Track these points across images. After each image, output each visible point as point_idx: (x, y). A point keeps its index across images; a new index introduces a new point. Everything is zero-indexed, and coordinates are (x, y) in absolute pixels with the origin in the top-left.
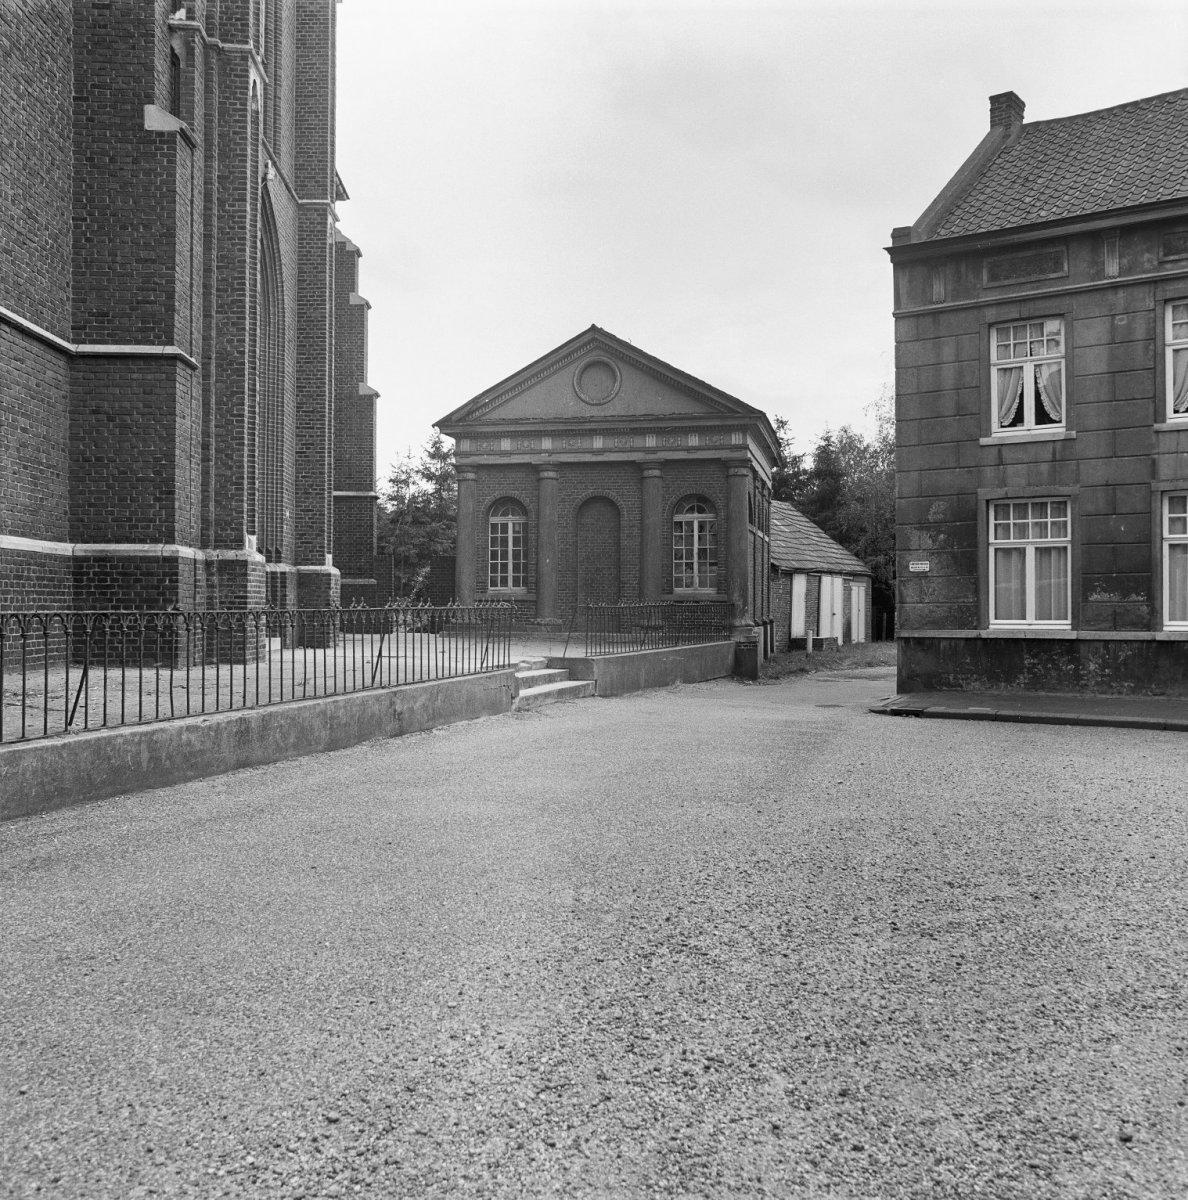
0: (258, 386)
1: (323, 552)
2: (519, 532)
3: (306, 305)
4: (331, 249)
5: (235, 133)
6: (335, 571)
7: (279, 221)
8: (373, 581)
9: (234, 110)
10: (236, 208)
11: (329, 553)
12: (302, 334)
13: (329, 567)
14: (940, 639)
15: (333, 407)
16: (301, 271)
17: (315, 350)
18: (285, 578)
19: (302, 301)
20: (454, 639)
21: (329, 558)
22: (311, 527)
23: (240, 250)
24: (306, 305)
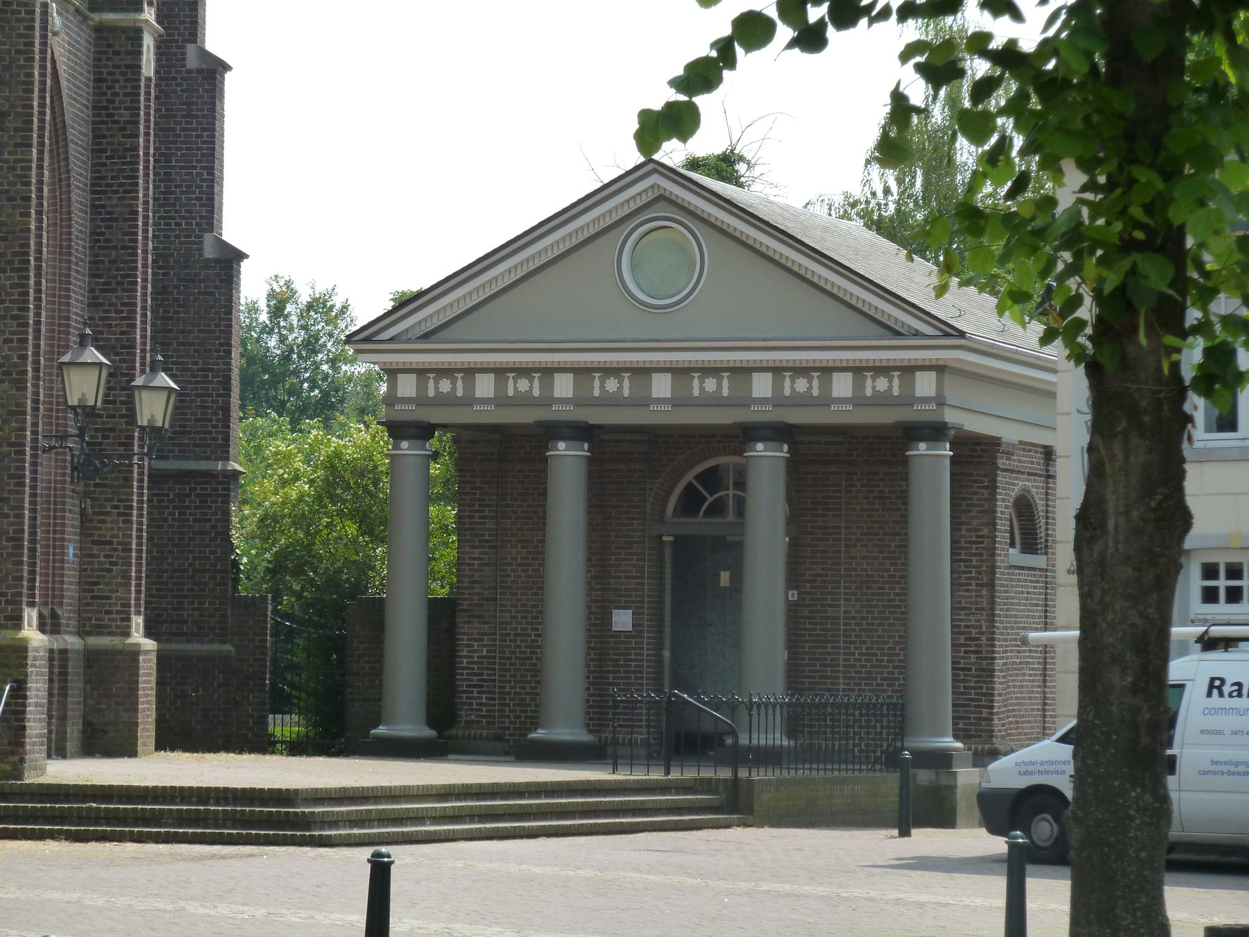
0: (42, 395)
1: (129, 613)
2: (821, 363)
3: (105, 192)
4: (148, 86)
5: (18, 52)
6: (149, 644)
7: (72, 133)
8: (228, 647)
9: (18, 20)
10: (19, 157)
11: (138, 613)
12: (98, 241)
13: (138, 638)
14: (297, 748)
15: (150, 277)
16: (97, 136)
17: (118, 269)
18: (67, 659)
19: (100, 185)
20: (764, 769)
21: (138, 621)
22: (109, 571)
23: (22, 215)
24: (105, 192)
